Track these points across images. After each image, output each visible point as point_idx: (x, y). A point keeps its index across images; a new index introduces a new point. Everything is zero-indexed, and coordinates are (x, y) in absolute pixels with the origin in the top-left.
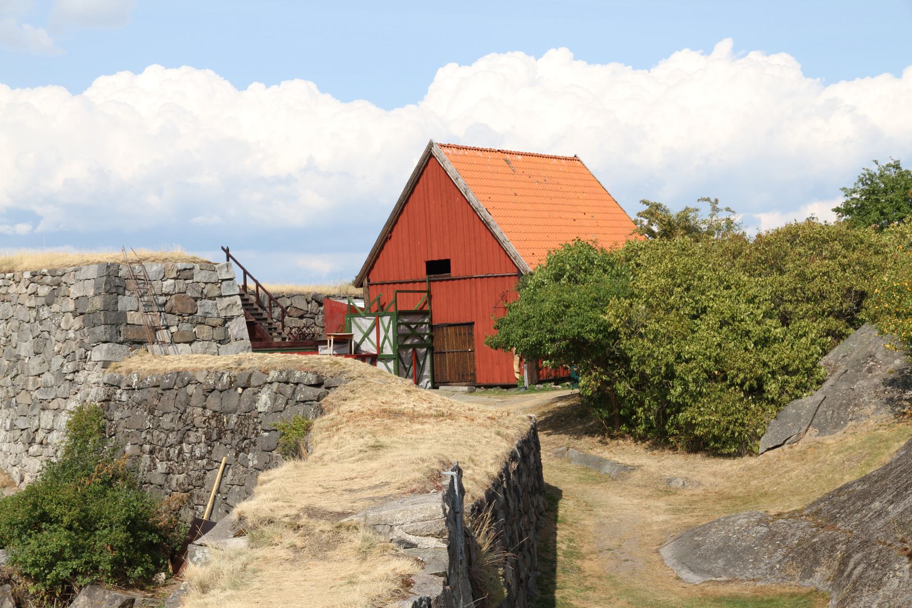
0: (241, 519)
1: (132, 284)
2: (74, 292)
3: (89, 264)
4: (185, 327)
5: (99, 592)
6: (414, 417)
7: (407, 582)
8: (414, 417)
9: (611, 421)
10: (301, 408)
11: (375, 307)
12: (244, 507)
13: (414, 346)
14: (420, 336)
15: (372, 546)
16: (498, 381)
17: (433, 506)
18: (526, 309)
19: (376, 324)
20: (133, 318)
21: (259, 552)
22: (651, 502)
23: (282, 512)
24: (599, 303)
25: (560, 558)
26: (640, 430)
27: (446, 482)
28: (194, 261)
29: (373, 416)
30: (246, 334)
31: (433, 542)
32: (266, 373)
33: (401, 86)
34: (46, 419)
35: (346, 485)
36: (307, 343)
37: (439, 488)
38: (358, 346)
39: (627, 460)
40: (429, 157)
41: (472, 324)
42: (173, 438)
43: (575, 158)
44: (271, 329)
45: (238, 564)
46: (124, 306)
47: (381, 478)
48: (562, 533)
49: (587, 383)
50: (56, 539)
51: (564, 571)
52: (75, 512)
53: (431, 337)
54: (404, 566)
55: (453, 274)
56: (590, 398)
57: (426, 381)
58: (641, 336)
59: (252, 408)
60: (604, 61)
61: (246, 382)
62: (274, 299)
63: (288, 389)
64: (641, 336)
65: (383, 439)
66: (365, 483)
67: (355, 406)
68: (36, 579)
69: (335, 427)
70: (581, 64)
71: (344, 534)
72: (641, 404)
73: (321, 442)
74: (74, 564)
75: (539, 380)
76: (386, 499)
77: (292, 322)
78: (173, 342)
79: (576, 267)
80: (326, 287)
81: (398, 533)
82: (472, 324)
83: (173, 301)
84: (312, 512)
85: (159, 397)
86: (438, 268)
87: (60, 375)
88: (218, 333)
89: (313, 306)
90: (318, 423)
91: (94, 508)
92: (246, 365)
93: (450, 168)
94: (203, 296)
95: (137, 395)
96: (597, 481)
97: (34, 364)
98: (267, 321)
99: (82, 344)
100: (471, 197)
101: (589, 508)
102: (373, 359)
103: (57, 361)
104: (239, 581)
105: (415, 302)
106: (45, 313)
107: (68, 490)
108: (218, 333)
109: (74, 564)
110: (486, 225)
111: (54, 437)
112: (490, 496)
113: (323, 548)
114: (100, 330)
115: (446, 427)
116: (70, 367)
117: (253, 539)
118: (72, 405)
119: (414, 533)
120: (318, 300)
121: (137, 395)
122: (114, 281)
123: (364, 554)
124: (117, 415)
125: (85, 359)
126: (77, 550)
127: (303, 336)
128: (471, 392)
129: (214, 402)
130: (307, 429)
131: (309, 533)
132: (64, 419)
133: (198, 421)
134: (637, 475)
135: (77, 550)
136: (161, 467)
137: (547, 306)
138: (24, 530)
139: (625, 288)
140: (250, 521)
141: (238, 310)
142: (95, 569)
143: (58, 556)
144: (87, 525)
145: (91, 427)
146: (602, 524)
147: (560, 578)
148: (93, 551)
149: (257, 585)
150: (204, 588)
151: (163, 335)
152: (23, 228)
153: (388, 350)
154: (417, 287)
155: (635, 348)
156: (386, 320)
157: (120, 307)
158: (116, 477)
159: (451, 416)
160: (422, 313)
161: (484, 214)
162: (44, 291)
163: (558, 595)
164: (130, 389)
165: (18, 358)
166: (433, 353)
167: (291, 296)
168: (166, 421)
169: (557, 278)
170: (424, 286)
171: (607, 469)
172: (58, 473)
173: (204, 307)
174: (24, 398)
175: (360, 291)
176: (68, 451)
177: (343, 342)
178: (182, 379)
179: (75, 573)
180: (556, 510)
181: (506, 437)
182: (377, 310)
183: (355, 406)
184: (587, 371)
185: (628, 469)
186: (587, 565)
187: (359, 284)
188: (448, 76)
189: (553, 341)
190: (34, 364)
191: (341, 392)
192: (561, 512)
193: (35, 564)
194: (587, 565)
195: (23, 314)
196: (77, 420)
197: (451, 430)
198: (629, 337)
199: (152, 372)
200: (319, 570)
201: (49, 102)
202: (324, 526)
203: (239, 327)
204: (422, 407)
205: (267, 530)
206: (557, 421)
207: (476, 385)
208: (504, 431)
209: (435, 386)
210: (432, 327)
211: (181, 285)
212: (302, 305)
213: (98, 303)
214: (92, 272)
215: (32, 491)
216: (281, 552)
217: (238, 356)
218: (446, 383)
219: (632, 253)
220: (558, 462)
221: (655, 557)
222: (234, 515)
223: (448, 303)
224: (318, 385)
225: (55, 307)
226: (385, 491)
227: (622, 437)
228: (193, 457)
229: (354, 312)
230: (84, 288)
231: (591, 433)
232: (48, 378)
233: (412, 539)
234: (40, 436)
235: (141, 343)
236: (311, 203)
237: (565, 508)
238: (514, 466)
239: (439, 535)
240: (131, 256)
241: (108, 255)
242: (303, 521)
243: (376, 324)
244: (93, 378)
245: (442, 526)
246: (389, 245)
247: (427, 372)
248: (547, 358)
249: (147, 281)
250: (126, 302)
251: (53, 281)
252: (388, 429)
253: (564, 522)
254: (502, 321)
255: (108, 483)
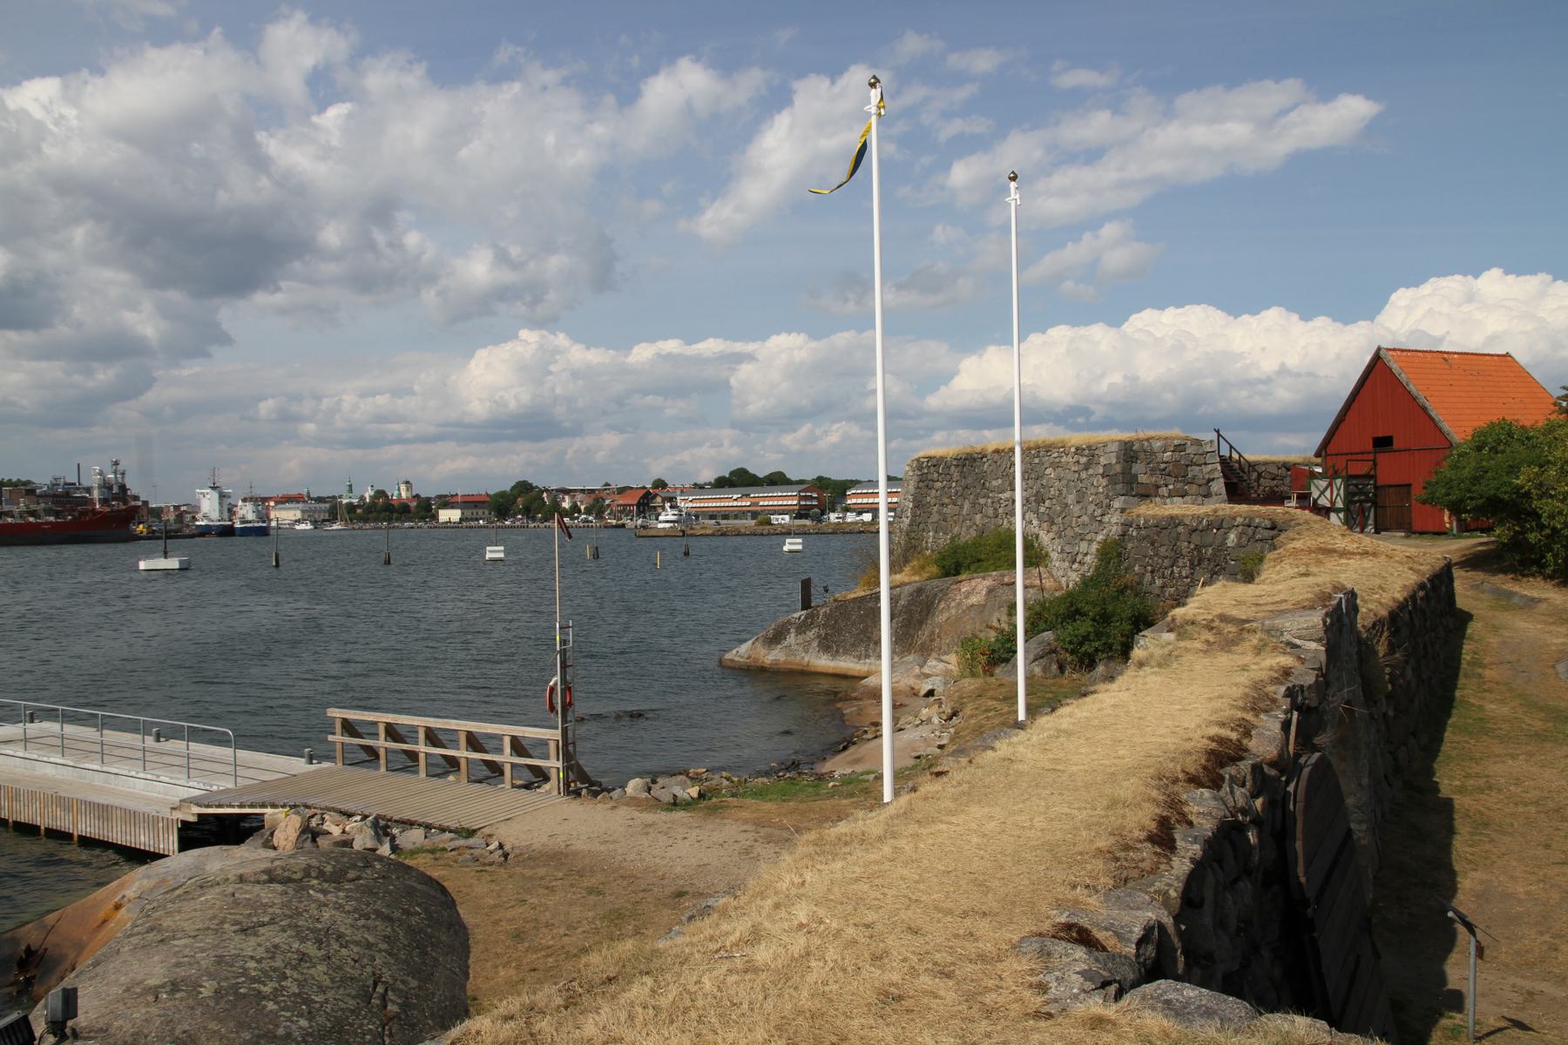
0: (1173, 620)
1: (1142, 456)
2: (1103, 461)
3: (1113, 441)
4: (1179, 485)
5: (1112, 664)
6: (1344, 554)
7: (1287, 672)
8: (1344, 554)
9: (1521, 563)
10: (1259, 545)
11: (1331, 472)
12: (1178, 612)
13: (1361, 502)
14: (1366, 494)
15: (1265, 645)
16: (1431, 529)
17: (1316, 618)
18: (1449, 474)
19: (1330, 485)
20: (1143, 478)
21: (1182, 644)
22: (1552, 628)
23: (1203, 616)
24: (1513, 470)
25: (1464, 665)
26: (1549, 571)
27: (1334, 602)
28: (1187, 439)
29: (1310, 551)
30: (1224, 491)
31: (1313, 645)
32: (1234, 519)
33: (1358, 304)
34: (1084, 546)
35: (1255, 600)
36: (1277, 498)
37: (1324, 606)
38: (1315, 501)
39: (1535, 594)
40: (1377, 359)
41: (1409, 485)
42: (1167, 563)
43: (1507, 355)
44: (1250, 488)
45: (1166, 651)
46: (1136, 467)
47: (1282, 597)
48: (1467, 647)
49: (1501, 533)
50: (1085, 627)
51: (1466, 676)
52: (1098, 609)
53: (1375, 495)
54: (1286, 660)
55: (1395, 446)
56: (1504, 545)
57: (1370, 529)
58: (1552, 497)
59: (1223, 543)
60: (1531, 270)
61: (1220, 524)
62: (1252, 466)
63: (1250, 531)
64: (1552, 497)
65: (1314, 569)
66: (1270, 600)
67: (1298, 544)
68: (1072, 652)
69: (1280, 560)
70: (1511, 278)
71: (1246, 635)
72: (1551, 550)
73: (1268, 572)
74: (1097, 644)
75: (1465, 529)
76: (1282, 612)
77: (1266, 483)
78: (1170, 496)
79: (1498, 440)
80: (1292, 458)
81: (1287, 637)
82: (1409, 485)
83: (1171, 467)
84: (1224, 618)
85: (1158, 534)
86: (1383, 443)
87: (1093, 517)
88: (1203, 490)
89: (1282, 471)
90: (1270, 556)
91: (1110, 608)
92: (1220, 513)
93: (1395, 367)
94: (1193, 464)
95: (1143, 532)
96: (1506, 609)
97: (1076, 509)
98: (1241, 481)
99: (1107, 497)
100: (1412, 388)
101: (1495, 629)
102: (1324, 512)
103: (1091, 508)
104: (1164, 663)
105: (1364, 468)
106: (1084, 475)
107: (1093, 594)
108: (1203, 490)
109: (1097, 644)
110: (1424, 409)
111: (1088, 559)
112: (1393, 616)
113: (1228, 644)
114: (1119, 487)
115: (1367, 563)
116: (1099, 512)
117: (1179, 634)
118: (1100, 537)
119: (1299, 638)
120: (1287, 466)
121: (1143, 532)
122: (1129, 453)
123: (1258, 650)
124: (1130, 546)
125: (1109, 506)
126: (1098, 635)
127: (1273, 492)
128: (1407, 537)
129: (1196, 538)
130: (1261, 560)
131: (1219, 633)
132: (1095, 546)
133: (1184, 552)
134: (1544, 606)
135: (1098, 635)
136: (1158, 582)
137: (1466, 473)
138: (1064, 619)
139: (1539, 457)
140: (1178, 622)
141: (1218, 474)
142: (1110, 648)
143: (1086, 638)
144: (1105, 618)
145: (1112, 553)
146: (1504, 643)
147: (1462, 681)
148: (1109, 636)
149: (1175, 665)
150: (1141, 665)
151: (1163, 491)
152: (1081, 420)
153: (1340, 504)
154: (1366, 457)
155: (1546, 507)
156: (1339, 481)
157: (1133, 471)
158: (1126, 587)
159: (1374, 555)
160: (1368, 476)
161: (1422, 400)
162: (1083, 460)
163: (1458, 694)
164: (1138, 528)
165: (1067, 505)
166: (1375, 507)
167: (1265, 463)
168: (1162, 550)
169: (1479, 449)
170: (1371, 457)
171: (1516, 600)
172: (1086, 583)
173: (1193, 471)
174: (1069, 532)
175: (1319, 460)
176: (1097, 568)
177: (1304, 499)
178: (1174, 522)
179: (1097, 650)
180: (1465, 629)
181: (1417, 572)
182: (1331, 475)
183: (1298, 544)
184: (1501, 522)
185: (1533, 601)
186: (1487, 673)
187: (1318, 455)
188: (1401, 297)
189: (1472, 499)
190: (1076, 509)
191: (1291, 534)
192: (1469, 631)
193: (1071, 642)
194: (1487, 673)
195: (1071, 476)
196: (1103, 548)
197: (1370, 565)
198: (1540, 497)
199: (1154, 517)
200: (1224, 660)
201: (1099, 335)
202: (1231, 628)
203: (1219, 486)
204: (1352, 547)
205: (1189, 628)
206: (1474, 562)
207: (1411, 531)
208: (1416, 566)
209: (1377, 532)
210: (1376, 488)
211: (1177, 455)
212: (1274, 470)
213: (1118, 468)
214: (1114, 448)
215: (1070, 594)
216: (1198, 645)
217: (1218, 506)
218: (1386, 530)
219: (1550, 429)
220: (1467, 591)
221: (1551, 671)
222: (1169, 619)
223: (1390, 469)
224: (1273, 528)
225: (1091, 471)
226: (1284, 606)
227: (1533, 575)
228: (1181, 577)
229: (1313, 475)
230: (1109, 458)
231: (1505, 572)
232: (1085, 518)
233: (1298, 642)
234: (1079, 558)
235: (1148, 496)
236: (1284, 396)
237: (1473, 628)
238: (1421, 594)
239: (1319, 640)
240: (1142, 435)
241: (1126, 436)
242: (1216, 624)
243: (1330, 485)
244: (1114, 520)
245: (1321, 634)
246: (1342, 426)
247: (1371, 521)
248: (1468, 512)
249: (1153, 453)
250: (1138, 468)
251: (1090, 453)
252: (1319, 562)
253: (1471, 639)
254: (1429, 483)
255: (1122, 592)
